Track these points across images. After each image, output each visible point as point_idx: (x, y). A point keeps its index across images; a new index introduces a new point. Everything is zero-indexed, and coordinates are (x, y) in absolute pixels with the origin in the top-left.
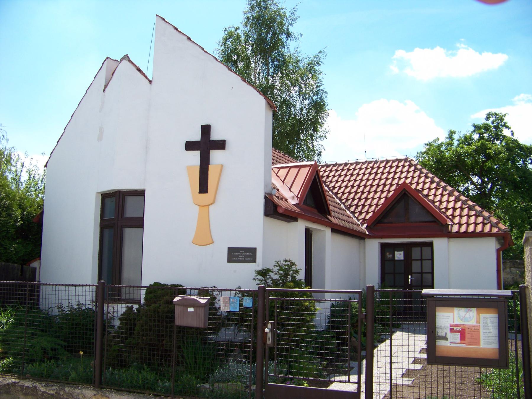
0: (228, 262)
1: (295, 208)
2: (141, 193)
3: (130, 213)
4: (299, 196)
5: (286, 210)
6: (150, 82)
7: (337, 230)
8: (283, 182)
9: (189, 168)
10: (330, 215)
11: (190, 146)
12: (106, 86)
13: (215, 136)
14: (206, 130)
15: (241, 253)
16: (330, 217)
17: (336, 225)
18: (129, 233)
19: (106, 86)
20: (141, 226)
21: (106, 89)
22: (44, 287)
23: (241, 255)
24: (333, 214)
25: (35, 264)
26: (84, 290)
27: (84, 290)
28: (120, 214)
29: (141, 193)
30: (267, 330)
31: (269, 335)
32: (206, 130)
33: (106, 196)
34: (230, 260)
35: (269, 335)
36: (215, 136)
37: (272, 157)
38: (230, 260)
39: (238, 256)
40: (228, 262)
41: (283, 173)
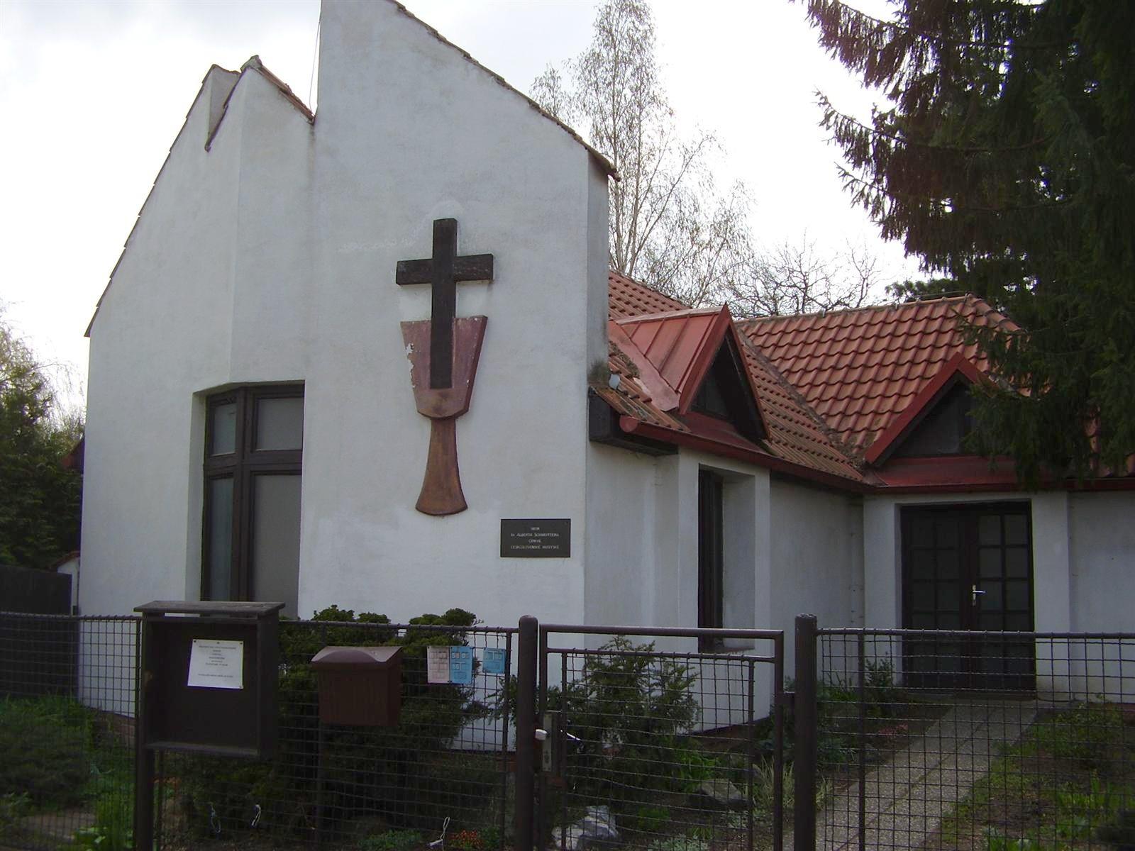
0: (502, 556)
1: (675, 425)
2: (293, 391)
3: (272, 440)
4: (680, 390)
5: (643, 425)
6: (312, 120)
7: (788, 477)
8: (645, 356)
9: (410, 329)
10: (766, 436)
11: (409, 274)
12: (212, 135)
13: (467, 245)
14: (445, 231)
15: (533, 532)
16: (766, 442)
17: (782, 462)
18: (269, 487)
19: (212, 135)
20: (298, 472)
21: (213, 145)
22: (87, 624)
23: (533, 538)
24: (773, 433)
25: (68, 568)
26: (110, 629)
27: (110, 629)
28: (248, 440)
29: (293, 391)
30: (541, 733)
31: (547, 749)
32: (445, 231)
33: (214, 401)
34: (506, 552)
35: (547, 749)
36: (467, 245)
37: (608, 290)
38: (506, 552)
39: (525, 541)
40: (502, 556)
41: (644, 336)
